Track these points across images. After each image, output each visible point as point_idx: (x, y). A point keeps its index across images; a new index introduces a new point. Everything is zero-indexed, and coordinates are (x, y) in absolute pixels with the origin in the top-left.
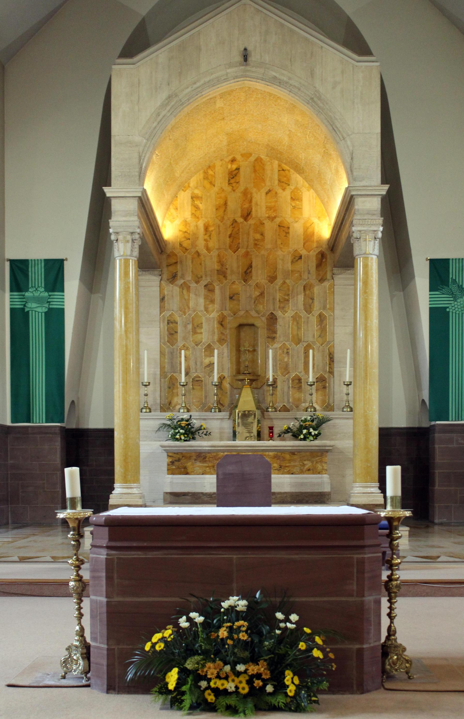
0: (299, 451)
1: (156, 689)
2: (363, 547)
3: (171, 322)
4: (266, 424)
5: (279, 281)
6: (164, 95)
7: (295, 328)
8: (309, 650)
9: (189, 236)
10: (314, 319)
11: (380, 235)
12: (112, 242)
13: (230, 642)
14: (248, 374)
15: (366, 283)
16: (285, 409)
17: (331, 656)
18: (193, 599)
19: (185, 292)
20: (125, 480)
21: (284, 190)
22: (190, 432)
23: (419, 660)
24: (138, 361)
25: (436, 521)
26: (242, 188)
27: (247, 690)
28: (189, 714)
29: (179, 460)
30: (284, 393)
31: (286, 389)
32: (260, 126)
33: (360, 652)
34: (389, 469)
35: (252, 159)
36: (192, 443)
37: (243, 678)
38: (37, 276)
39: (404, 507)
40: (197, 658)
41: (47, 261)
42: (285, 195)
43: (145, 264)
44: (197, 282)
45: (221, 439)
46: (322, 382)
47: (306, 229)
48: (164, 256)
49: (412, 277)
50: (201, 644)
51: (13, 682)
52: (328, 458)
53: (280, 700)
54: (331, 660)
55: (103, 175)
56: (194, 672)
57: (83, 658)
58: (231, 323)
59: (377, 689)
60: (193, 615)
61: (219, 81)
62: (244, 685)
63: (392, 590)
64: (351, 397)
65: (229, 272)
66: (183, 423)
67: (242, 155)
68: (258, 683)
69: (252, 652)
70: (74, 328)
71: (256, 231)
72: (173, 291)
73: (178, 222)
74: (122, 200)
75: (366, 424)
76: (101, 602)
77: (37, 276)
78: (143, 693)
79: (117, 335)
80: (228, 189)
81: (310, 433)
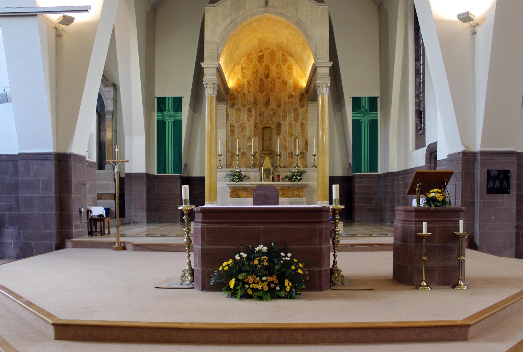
0: (292, 187)
1: (224, 288)
2: (322, 222)
3: (232, 126)
4: (276, 174)
5: (282, 107)
6: (229, 20)
7: (290, 129)
8: (296, 269)
9: (240, 86)
10: (298, 125)
11: (329, 85)
12: (204, 88)
13: (259, 266)
14: (267, 150)
15: (323, 107)
16: (285, 167)
17: (307, 273)
18: (242, 247)
19: (238, 112)
20: (210, 200)
21: (284, 65)
22: (241, 178)
23: (348, 277)
24: (216, 144)
25: (356, 220)
26: (265, 64)
27: (267, 289)
28: (240, 300)
29: (235, 191)
30: (285, 160)
31: (285, 158)
32: (273, 35)
33: (320, 272)
34: (334, 186)
35: (270, 50)
36: (241, 183)
37: (266, 283)
38: (169, 105)
39: (341, 203)
40: (244, 274)
41: (174, 98)
42: (285, 67)
43: (220, 99)
44: (244, 107)
45: (255, 181)
46: (302, 154)
47: (295, 83)
48: (229, 95)
49: (344, 105)
50: (246, 267)
51: (158, 286)
52: (305, 190)
53: (283, 293)
54: (307, 275)
55: (200, 57)
56: (243, 280)
57: (190, 275)
58: (260, 127)
59: (328, 289)
60: (242, 254)
61: (254, 14)
62: (266, 286)
63: (336, 246)
64: (316, 162)
65: (259, 102)
66: (237, 174)
67: (265, 49)
68: (272, 285)
69: (270, 271)
70: (187, 128)
71: (271, 84)
72: (233, 112)
73: (235, 79)
74: (209, 69)
75: (323, 174)
76: (199, 248)
77: (169, 105)
78: (219, 291)
79: (206, 132)
80: (258, 64)
81: (297, 178)
